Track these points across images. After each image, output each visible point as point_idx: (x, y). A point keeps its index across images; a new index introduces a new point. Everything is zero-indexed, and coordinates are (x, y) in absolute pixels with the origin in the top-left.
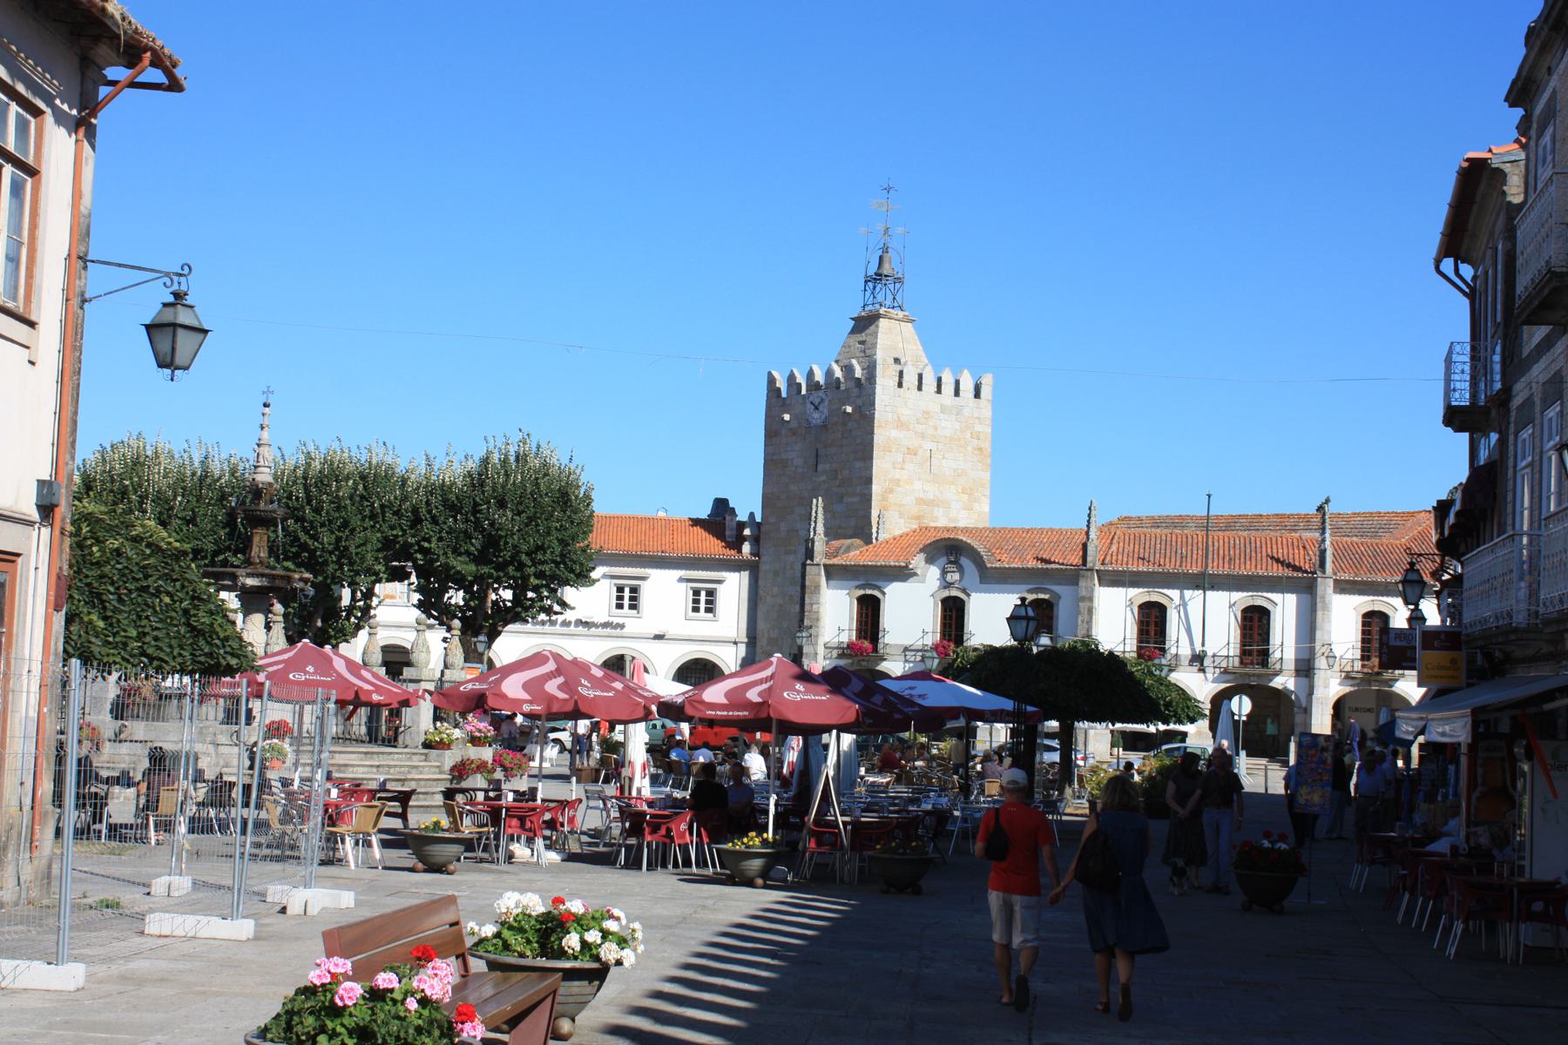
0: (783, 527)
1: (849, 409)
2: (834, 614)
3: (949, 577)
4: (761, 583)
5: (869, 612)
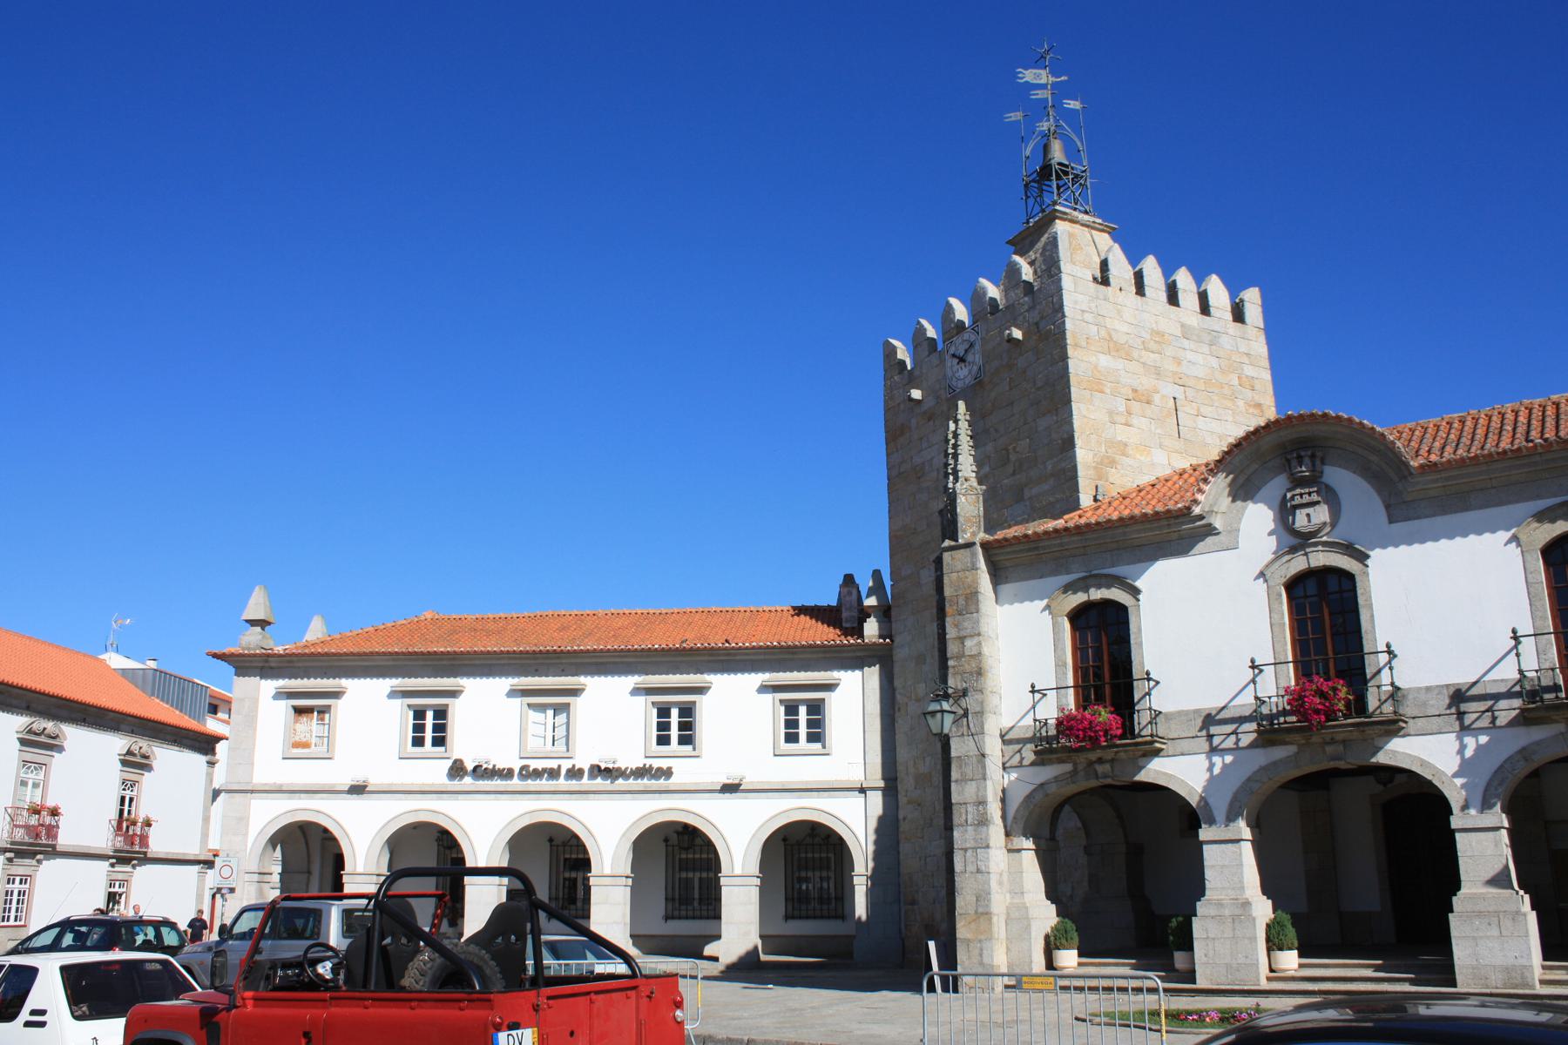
1: (1017, 334)
2: (1019, 655)
3: (1301, 520)
4: (897, 683)
5: (1104, 648)
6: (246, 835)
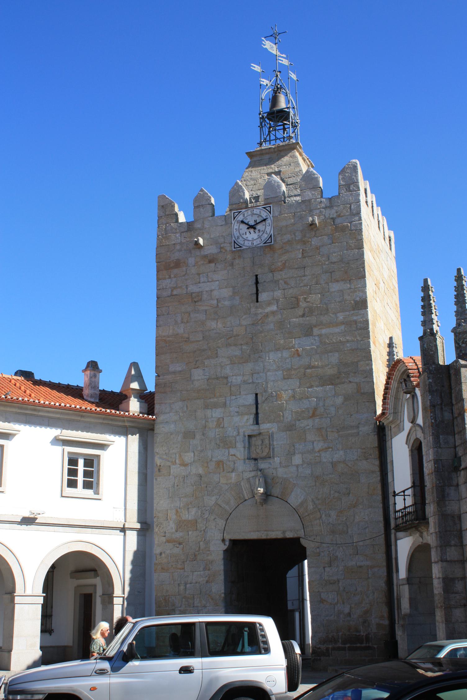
0: (198, 375)
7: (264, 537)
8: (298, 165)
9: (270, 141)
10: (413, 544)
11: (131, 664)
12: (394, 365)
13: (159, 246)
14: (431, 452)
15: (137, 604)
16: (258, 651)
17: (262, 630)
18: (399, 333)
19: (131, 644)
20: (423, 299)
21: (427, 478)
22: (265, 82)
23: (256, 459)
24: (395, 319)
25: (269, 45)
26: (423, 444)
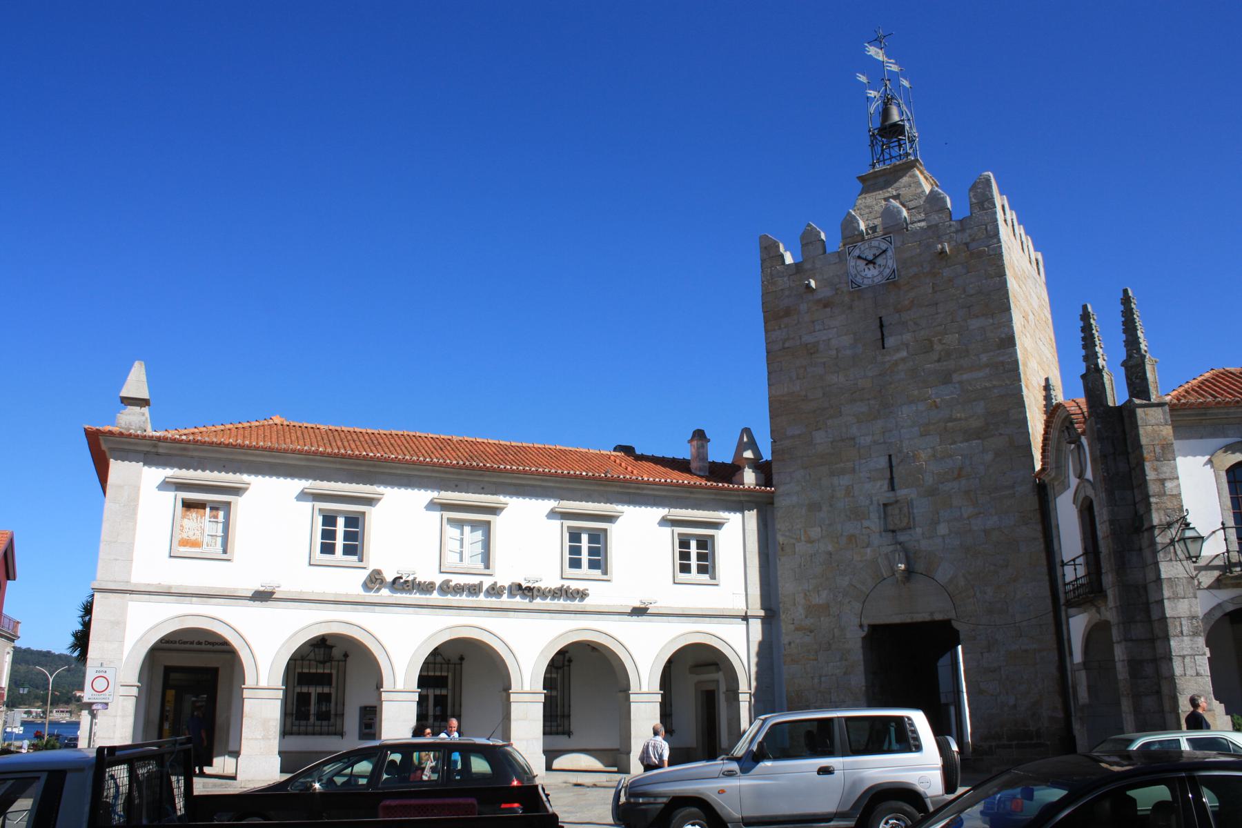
0: (820, 437)
6: (122, 641)
7: (909, 620)
8: (919, 184)
9: (884, 161)
10: (1089, 622)
11: (762, 764)
12: (1052, 411)
13: (765, 294)
14: (1105, 511)
15: (763, 703)
16: (908, 749)
17: (912, 725)
18: (1057, 373)
19: (760, 744)
20: (1083, 330)
21: (1100, 534)
22: (872, 94)
23: (893, 531)
24: (1049, 356)
25: (874, 52)
26: (1095, 504)
